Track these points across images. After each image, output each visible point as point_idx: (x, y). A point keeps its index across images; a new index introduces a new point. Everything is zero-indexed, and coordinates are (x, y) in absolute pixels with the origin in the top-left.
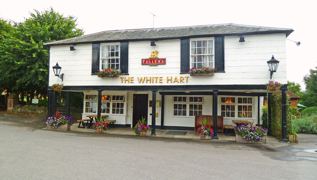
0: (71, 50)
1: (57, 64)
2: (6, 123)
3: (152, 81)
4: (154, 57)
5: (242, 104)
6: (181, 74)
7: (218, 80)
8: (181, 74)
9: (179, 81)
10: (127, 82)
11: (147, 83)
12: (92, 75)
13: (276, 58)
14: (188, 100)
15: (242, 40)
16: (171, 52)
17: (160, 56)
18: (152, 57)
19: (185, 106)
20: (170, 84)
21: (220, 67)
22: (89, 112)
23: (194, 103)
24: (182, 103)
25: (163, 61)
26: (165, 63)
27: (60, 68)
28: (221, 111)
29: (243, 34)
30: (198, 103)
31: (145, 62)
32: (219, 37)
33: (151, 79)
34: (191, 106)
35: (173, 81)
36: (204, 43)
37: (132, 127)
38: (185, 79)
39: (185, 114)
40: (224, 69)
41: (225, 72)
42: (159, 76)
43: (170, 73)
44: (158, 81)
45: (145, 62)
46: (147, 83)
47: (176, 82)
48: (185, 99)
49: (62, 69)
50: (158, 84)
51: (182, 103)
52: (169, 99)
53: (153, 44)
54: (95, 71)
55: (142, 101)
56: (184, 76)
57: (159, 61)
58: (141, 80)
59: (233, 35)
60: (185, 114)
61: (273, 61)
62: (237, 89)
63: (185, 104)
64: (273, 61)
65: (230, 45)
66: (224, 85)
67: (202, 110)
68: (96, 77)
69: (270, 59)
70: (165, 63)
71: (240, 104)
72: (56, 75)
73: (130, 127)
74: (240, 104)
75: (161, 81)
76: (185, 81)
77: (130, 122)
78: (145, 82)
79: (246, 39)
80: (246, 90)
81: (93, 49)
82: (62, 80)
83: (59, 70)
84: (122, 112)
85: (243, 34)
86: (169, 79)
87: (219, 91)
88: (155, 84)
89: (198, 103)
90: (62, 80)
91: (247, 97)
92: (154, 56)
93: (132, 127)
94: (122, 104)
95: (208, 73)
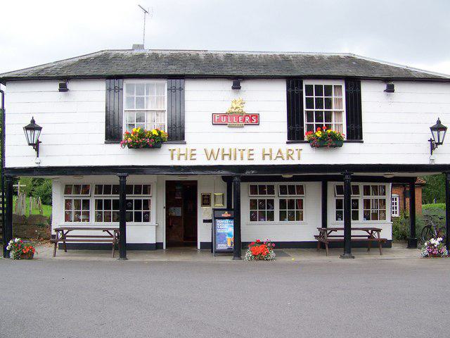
0: (60, 91)
1: (33, 121)
2: (80, 258)
3: (232, 156)
4: (237, 110)
5: (371, 197)
6: (287, 143)
7: (349, 155)
8: (287, 143)
9: (285, 157)
10: (182, 157)
11: (223, 159)
12: (106, 143)
13: (38, 123)
14: (277, 190)
15: (390, 90)
16: (270, 101)
17: (249, 109)
18: (233, 110)
19: (271, 202)
20: (267, 162)
21: (355, 133)
22: (259, 220)
23: (288, 197)
24: (266, 197)
25: (254, 119)
26: (257, 123)
27: (40, 129)
28: (335, 210)
29: (391, 79)
30: (295, 197)
31: (221, 120)
32: (354, 78)
33: (232, 152)
34: (282, 203)
35: (274, 157)
36: (320, 92)
37: (164, 247)
38: (296, 152)
39: (271, 217)
40: (183, 138)
41: (363, 142)
42: (248, 147)
43: (267, 141)
44: (246, 157)
45: (221, 120)
46: (223, 159)
47: (281, 159)
48: (271, 191)
49: (448, 131)
50: (246, 162)
51: (266, 197)
52: (245, 188)
53: (236, 87)
54: (113, 135)
55: (183, 192)
56: (294, 147)
57: (247, 119)
58: (212, 153)
59: (217, 78)
60: (271, 217)
61: (439, 127)
62: (379, 171)
63: (272, 198)
64: (439, 127)
65: (371, 95)
66: (117, 167)
67: (304, 210)
68: (116, 148)
69: (434, 123)
70: (257, 123)
71: (367, 197)
72: (30, 144)
73: (162, 248)
74: (367, 197)
75: (251, 157)
76: (295, 156)
77: (163, 239)
78: (220, 157)
79: (397, 87)
80: (386, 173)
81: (109, 90)
82: (38, 153)
83: (442, 133)
84: (147, 220)
85: (391, 79)
86: (267, 152)
87: (355, 174)
88: (238, 162)
89: (295, 197)
90: (38, 153)
91: (378, 184)
92: (237, 108)
93: (164, 247)
94: (147, 203)
95: (331, 142)
